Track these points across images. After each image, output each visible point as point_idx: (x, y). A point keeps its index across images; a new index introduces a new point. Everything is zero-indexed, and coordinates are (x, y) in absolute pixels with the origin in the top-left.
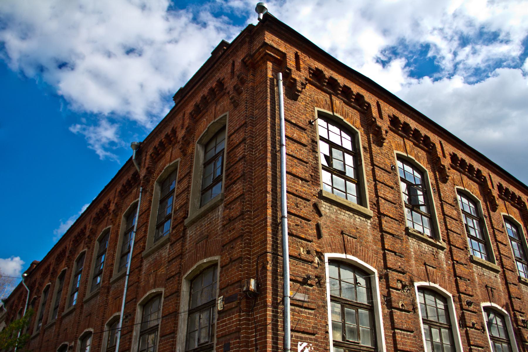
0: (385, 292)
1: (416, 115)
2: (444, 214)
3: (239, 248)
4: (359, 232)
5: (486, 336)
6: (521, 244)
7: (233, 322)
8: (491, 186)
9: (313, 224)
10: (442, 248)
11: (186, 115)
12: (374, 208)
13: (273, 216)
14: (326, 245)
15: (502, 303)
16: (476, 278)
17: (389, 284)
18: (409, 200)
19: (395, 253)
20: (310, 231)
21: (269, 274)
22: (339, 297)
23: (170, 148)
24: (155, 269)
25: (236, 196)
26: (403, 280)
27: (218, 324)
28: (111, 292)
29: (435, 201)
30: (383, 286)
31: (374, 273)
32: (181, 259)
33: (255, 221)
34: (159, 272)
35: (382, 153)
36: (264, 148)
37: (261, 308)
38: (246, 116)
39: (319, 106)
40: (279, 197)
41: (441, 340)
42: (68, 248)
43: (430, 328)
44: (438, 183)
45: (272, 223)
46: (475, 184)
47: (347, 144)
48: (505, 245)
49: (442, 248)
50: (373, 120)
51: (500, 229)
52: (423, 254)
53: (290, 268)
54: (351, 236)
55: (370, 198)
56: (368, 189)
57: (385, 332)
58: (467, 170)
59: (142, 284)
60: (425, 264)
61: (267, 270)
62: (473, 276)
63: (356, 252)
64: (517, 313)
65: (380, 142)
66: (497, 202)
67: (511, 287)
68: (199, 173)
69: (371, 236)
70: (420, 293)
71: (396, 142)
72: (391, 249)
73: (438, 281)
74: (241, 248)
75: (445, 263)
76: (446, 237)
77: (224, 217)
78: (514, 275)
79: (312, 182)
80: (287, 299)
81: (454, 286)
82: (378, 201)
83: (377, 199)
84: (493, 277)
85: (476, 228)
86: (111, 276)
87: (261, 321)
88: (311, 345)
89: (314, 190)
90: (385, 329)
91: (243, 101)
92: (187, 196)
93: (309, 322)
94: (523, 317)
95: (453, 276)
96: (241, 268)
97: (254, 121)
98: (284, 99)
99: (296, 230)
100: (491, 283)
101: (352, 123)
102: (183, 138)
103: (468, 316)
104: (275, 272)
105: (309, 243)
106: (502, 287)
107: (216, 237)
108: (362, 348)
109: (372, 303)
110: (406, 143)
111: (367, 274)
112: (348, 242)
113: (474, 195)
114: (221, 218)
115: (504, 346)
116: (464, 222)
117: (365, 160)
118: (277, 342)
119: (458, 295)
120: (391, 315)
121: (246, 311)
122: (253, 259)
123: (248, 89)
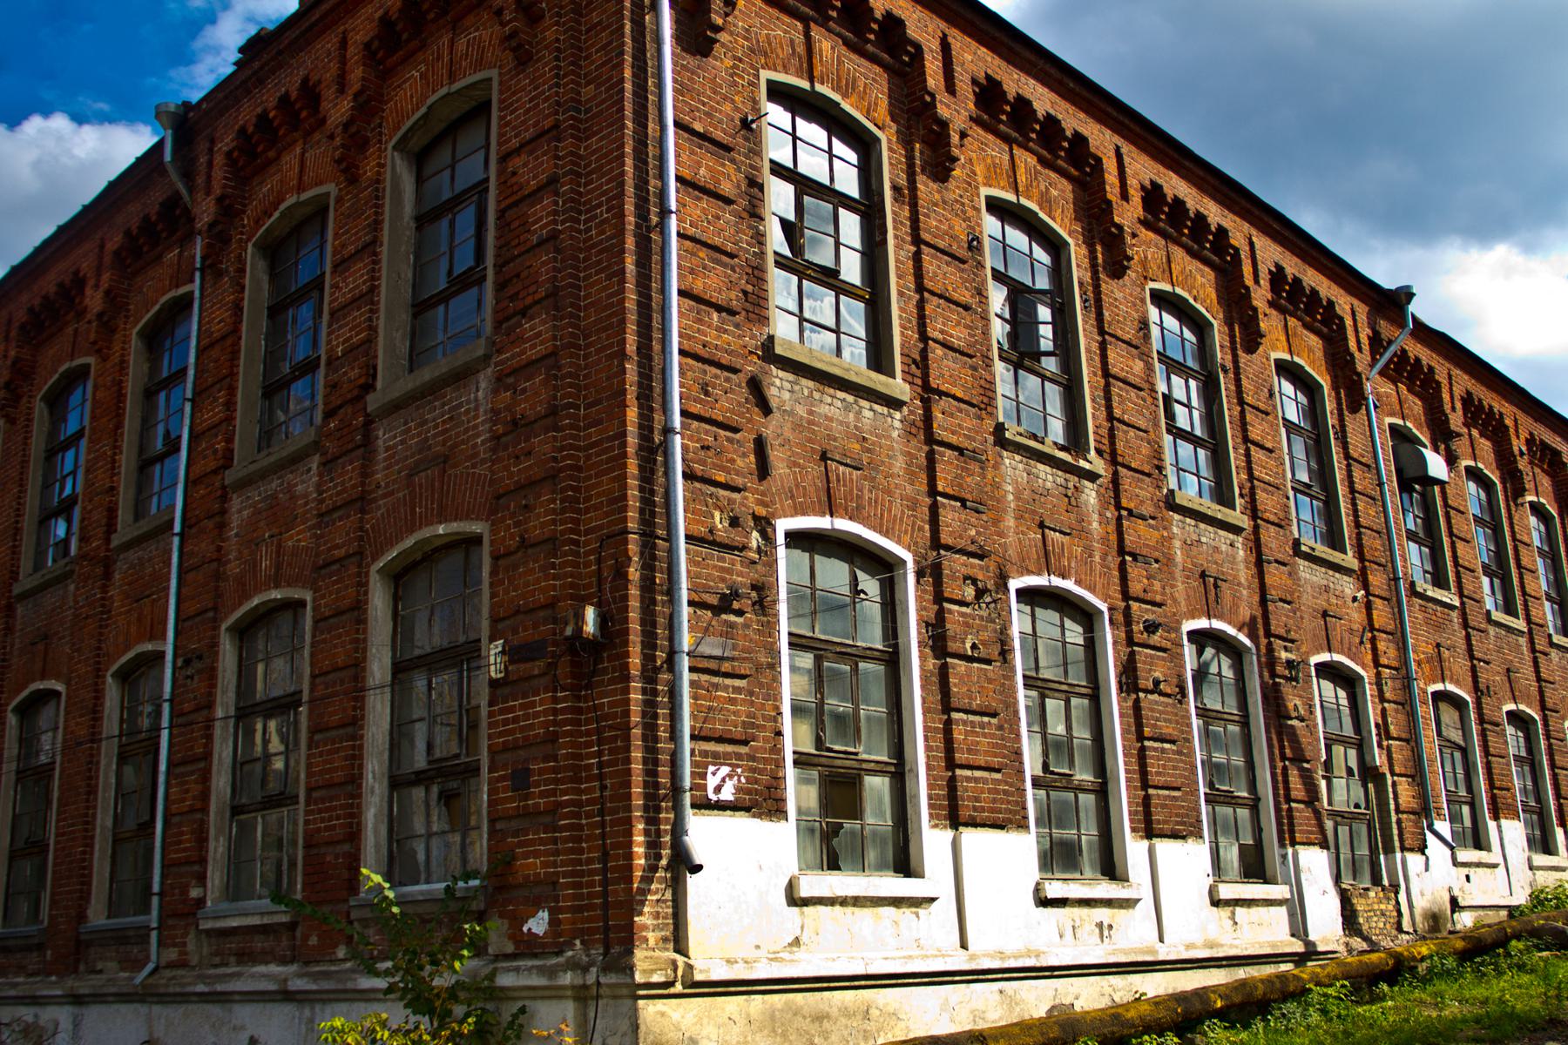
0: (931, 615)
1: (1053, 71)
2: (1106, 374)
3: (547, 513)
4: (868, 451)
5: (1188, 711)
6: (1317, 442)
7: (536, 715)
8: (1251, 277)
9: (747, 437)
10: (1092, 476)
11: (351, 50)
12: (913, 375)
13: (641, 427)
14: (780, 495)
15: (1241, 618)
16: (1179, 552)
17: (942, 592)
18: (1013, 337)
19: (963, 501)
20: (740, 462)
21: (634, 592)
22: (811, 634)
23: (295, 141)
24: (275, 531)
25: (532, 354)
26: (980, 577)
27: (491, 714)
28: (117, 576)
29: (1085, 336)
30: (927, 597)
31: (904, 562)
32: (363, 511)
33: (590, 436)
34: (291, 537)
35: (944, 202)
36: (614, 216)
37: (612, 681)
38: (558, 103)
39: (770, 64)
40: (657, 368)
41: (1069, 728)
43: (1043, 697)
44: (1098, 279)
45: (641, 448)
46: (1207, 269)
47: (848, 182)
48: (1270, 451)
49: (1092, 476)
50: (928, 99)
51: (1261, 406)
52: (1037, 497)
53: (688, 572)
54: (846, 465)
55: (903, 346)
56: (900, 317)
57: (925, 721)
58: (1186, 231)
59: (233, 568)
60: (1042, 525)
61: (628, 581)
62: (1169, 548)
63: (859, 508)
64: (1278, 643)
65: (941, 168)
66: (1262, 324)
67: (1273, 572)
68: (403, 248)
69: (900, 458)
70: (1022, 606)
71: (989, 161)
72: (952, 492)
73: (1073, 571)
74: (554, 511)
75: (1096, 516)
76: (1106, 442)
77: (495, 412)
78: (1284, 536)
79: (747, 311)
80: (682, 660)
81: (1117, 581)
82: (924, 353)
83: (922, 346)
84: (1224, 548)
85: (1195, 403)
86: (111, 528)
87: (615, 716)
88: (739, 770)
89: (752, 337)
90: (926, 711)
91: (546, 47)
92: (370, 319)
93: (734, 713)
94: (1291, 652)
95: (1115, 553)
96: (554, 569)
97: (580, 121)
98: (673, 54)
99: (704, 463)
100: (1216, 563)
101: (865, 110)
102: (346, 126)
103: (1145, 663)
104: (648, 586)
105: (735, 496)
106: (1244, 574)
107: (474, 466)
108: (864, 766)
109: (896, 646)
110: (1018, 161)
111: (883, 565)
112: (838, 481)
113: (1198, 306)
114: (486, 412)
115: (1232, 732)
116: (1162, 387)
117: (895, 228)
118: (657, 771)
119: (1123, 604)
120: (944, 673)
121: (572, 688)
122: (587, 543)
123: (562, 8)
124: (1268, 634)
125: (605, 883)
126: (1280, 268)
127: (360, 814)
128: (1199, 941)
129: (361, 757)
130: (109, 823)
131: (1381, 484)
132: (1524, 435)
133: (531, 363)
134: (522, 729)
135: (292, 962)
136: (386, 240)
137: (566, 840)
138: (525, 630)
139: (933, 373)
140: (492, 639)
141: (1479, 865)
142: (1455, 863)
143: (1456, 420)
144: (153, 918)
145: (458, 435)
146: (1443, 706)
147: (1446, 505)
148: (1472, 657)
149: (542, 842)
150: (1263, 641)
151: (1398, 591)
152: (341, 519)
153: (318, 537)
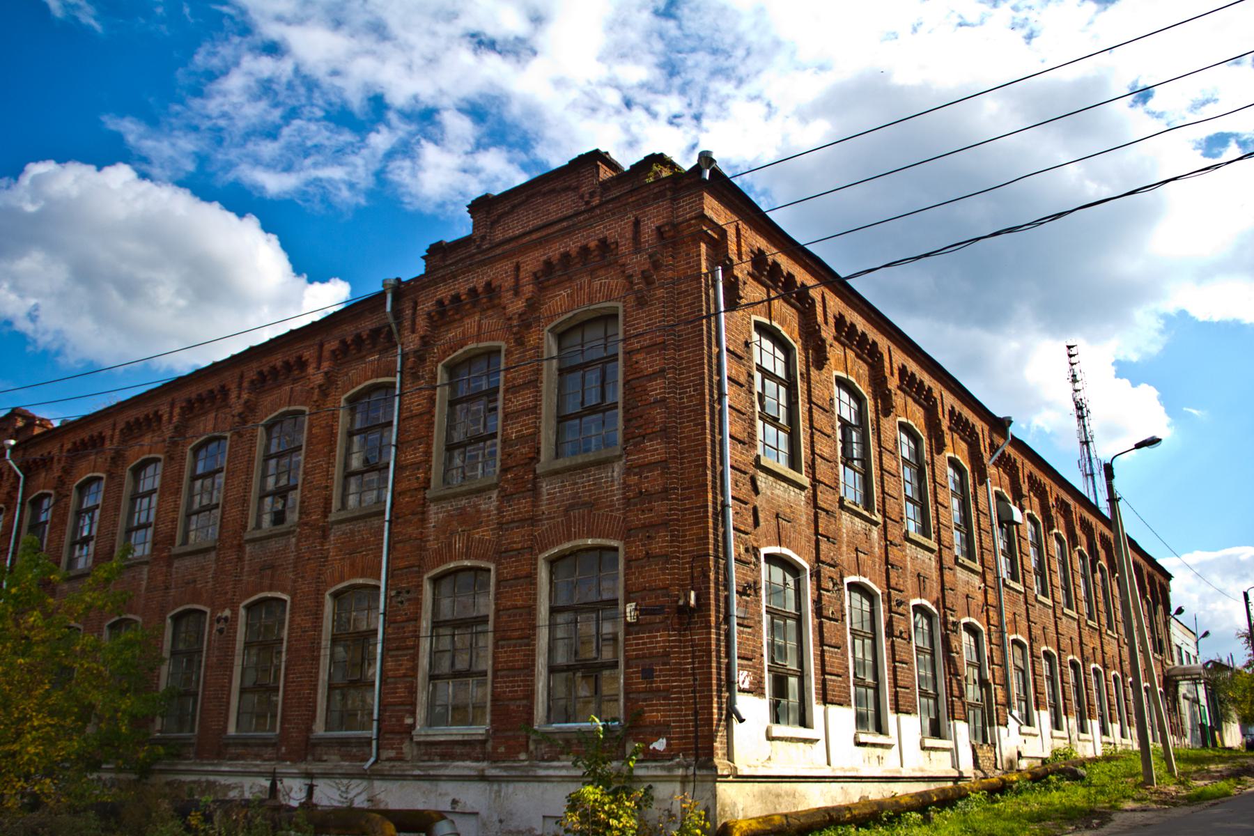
0: (815, 597)
3: (663, 542)
4: (793, 512)
10: (876, 524)
21: (712, 585)
36: (698, 394)
41: (864, 655)
42: (165, 417)
49: (876, 524)
60: (857, 550)
64: (949, 612)
67: (946, 572)
74: (667, 541)
90: (814, 645)
106: (935, 575)
107: (611, 511)
116: (757, 388)
120: (821, 625)
121: (679, 630)
124: (944, 607)
125: (696, 726)
126: (904, 367)
127: (533, 685)
128: (917, 768)
129: (534, 655)
130: (326, 678)
131: (992, 525)
132: (1054, 496)
133: (650, 464)
134: (648, 649)
135: (483, 760)
136: (545, 380)
137: (676, 704)
138: (650, 599)
139: (817, 472)
140: (627, 601)
141: (1030, 734)
142: (1020, 733)
143: (1025, 488)
144: (374, 733)
145: (599, 493)
146: (1015, 647)
147: (1019, 535)
148: (1029, 620)
149: (662, 705)
150: (942, 611)
151: (999, 584)
152: (517, 528)
153: (500, 536)
